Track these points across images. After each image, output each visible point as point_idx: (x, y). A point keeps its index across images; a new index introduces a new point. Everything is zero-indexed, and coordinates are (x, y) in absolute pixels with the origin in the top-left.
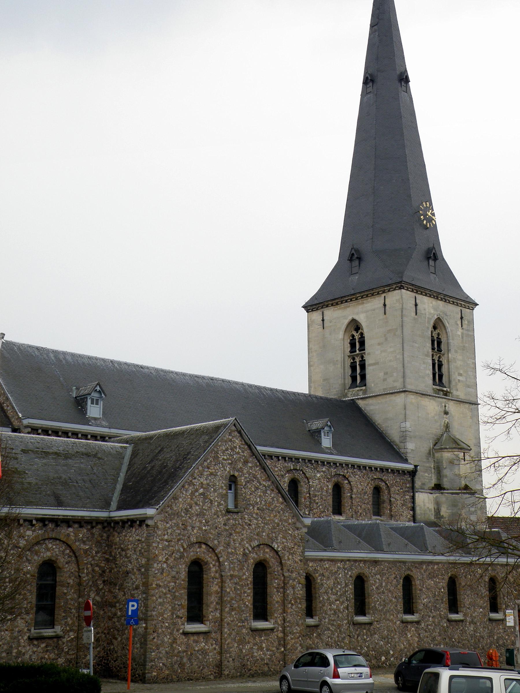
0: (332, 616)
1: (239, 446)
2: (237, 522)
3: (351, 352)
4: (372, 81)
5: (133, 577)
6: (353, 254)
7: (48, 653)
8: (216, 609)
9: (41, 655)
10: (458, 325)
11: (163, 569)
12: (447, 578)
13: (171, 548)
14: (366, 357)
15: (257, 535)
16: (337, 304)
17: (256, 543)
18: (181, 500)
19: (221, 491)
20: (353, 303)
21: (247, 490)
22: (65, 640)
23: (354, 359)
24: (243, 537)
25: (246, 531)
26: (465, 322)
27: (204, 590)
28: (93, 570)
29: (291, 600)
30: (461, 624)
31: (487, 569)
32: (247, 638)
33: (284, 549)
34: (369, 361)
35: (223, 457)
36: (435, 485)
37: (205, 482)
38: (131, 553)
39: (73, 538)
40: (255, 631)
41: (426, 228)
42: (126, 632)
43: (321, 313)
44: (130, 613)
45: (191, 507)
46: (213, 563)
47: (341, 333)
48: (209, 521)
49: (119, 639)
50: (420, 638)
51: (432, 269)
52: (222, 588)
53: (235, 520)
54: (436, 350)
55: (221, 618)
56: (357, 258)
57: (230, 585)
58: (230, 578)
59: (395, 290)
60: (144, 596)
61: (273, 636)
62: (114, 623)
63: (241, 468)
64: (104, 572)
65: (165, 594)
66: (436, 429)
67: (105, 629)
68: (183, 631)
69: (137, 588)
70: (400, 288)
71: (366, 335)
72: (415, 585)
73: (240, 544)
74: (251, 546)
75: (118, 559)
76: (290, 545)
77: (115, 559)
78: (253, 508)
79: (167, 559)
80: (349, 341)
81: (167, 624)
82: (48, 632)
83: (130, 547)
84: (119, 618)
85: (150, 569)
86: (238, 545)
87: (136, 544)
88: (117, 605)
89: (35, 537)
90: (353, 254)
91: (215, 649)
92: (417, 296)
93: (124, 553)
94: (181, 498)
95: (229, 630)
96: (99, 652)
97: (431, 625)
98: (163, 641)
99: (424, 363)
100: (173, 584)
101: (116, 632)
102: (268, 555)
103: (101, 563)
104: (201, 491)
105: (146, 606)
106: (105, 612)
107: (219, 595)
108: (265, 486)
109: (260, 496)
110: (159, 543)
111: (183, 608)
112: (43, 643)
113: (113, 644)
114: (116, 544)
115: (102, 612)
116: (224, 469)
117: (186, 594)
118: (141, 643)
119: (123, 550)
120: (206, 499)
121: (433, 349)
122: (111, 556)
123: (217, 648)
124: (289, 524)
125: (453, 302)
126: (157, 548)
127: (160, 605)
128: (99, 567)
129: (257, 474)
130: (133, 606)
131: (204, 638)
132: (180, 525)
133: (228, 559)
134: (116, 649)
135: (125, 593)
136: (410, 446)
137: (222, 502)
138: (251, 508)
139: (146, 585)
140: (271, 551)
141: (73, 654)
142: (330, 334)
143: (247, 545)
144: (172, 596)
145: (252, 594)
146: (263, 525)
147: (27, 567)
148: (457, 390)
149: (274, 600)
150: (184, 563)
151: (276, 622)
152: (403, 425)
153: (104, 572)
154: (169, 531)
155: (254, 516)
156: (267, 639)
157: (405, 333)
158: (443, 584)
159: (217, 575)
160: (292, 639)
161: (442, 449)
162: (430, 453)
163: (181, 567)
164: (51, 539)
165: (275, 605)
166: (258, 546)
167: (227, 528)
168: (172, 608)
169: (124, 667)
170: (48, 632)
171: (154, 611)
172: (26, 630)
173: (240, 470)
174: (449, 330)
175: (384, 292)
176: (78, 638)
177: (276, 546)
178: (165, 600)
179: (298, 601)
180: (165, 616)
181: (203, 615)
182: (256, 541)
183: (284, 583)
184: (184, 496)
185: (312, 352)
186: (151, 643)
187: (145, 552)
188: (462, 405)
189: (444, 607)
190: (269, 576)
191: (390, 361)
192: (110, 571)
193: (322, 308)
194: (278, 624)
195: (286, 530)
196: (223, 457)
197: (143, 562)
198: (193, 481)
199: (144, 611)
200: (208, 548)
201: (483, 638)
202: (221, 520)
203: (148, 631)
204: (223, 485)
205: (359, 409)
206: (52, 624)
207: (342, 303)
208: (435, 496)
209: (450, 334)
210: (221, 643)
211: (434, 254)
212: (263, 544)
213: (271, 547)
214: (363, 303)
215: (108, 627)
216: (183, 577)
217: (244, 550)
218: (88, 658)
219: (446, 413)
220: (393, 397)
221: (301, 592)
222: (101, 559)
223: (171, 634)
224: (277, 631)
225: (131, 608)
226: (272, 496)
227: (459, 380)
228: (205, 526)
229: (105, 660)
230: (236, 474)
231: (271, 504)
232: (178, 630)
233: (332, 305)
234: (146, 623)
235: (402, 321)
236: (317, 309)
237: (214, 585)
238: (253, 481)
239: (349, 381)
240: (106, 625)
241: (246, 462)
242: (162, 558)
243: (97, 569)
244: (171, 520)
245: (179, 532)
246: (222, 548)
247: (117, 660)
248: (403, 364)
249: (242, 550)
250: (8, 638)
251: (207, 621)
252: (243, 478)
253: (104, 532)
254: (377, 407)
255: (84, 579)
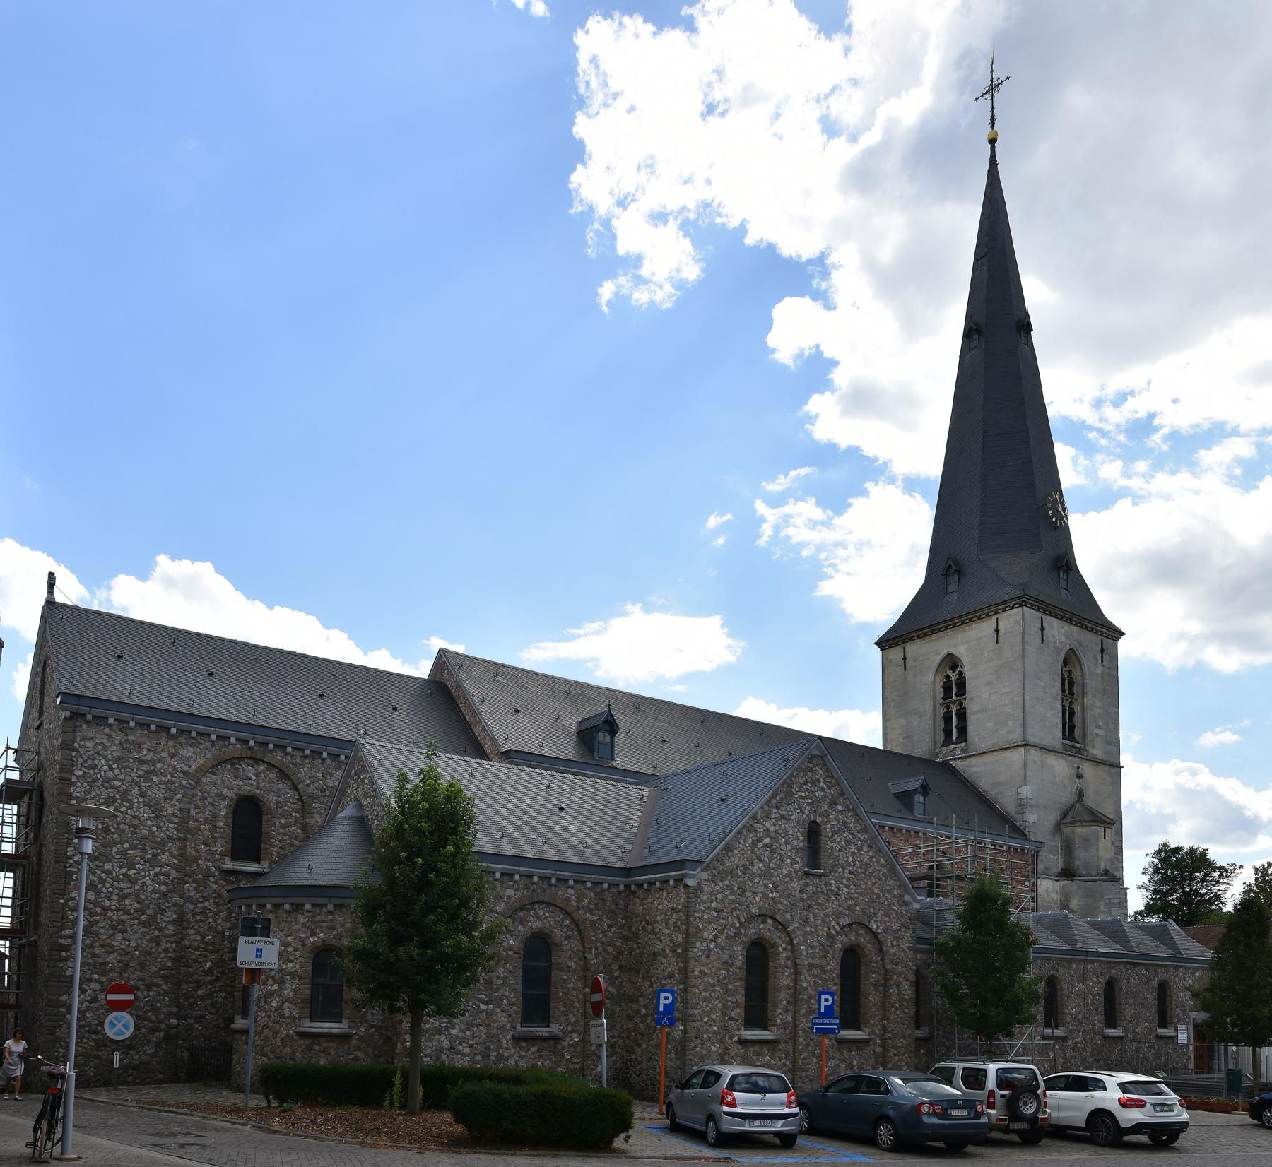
0: (948, 1027)
1: (824, 779)
2: (819, 889)
3: (944, 699)
4: (979, 331)
5: (664, 961)
6: (950, 567)
7: (542, 1060)
8: (788, 1011)
9: (532, 1062)
10: (1097, 659)
11: (710, 950)
12: (1103, 980)
13: (721, 921)
14: (965, 704)
15: (849, 909)
16: (926, 635)
17: (846, 921)
18: (736, 852)
19: (796, 842)
20: (950, 632)
21: (834, 845)
22: (565, 1043)
23: (948, 707)
24: (827, 911)
25: (833, 903)
26: (1106, 657)
27: (769, 983)
28: (605, 951)
29: (895, 1003)
30: (1119, 1041)
31: (1156, 972)
32: (830, 1051)
33: (886, 931)
34: (971, 708)
35: (799, 793)
36: (1062, 869)
37: (773, 828)
38: (660, 927)
39: (575, 904)
40: (843, 1042)
41: (1055, 527)
42: (654, 1036)
43: (902, 650)
44: (661, 1009)
45: (752, 864)
46: (784, 946)
47: (931, 673)
48: (778, 886)
49: (644, 1046)
50: (1066, 1058)
51: (1063, 584)
52: (796, 981)
53: (817, 886)
54: (1067, 693)
55: (794, 1023)
56: (956, 570)
57: (809, 978)
58: (808, 967)
59: (1013, 608)
60: (681, 987)
61: (868, 1051)
62: (637, 1024)
63: (826, 811)
64: (620, 953)
65: (713, 986)
66: (1066, 796)
67: (623, 1032)
68: (739, 1039)
69: (670, 976)
70: (1021, 606)
71: (967, 675)
72: (1062, 990)
73: (823, 921)
74: (838, 924)
75: (642, 936)
76: (895, 926)
77: (637, 936)
78: (843, 870)
79: (716, 937)
80: (941, 684)
81: (715, 1028)
82: (543, 1031)
83: (659, 918)
84: (644, 1017)
85: (691, 949)
86: (820, 922)
87: (669, 913)
88: (641, 999)
89: (520, 899)
90: (950, 567)
91: (785, 1065)
92: (1044, 617)
93: (650, 927)
94: (736, 849)
95: (805, 1040)
96: (615, 1062)
97: (1081, 1043)
98: (709, 1051)
99: (1052, 709)
100: (724, 972)
101: (639, 1037)
102: (863, 938)
103: (616, 941)
104: (767, 840)
105: (685, 1002)
106: (623, 1009)
107: (792, 991)
108: (860, 839)
109: (853, 854)
110: (703, 912)
111: (738, 1006)
112: (534, 1045)
113: (635, 1053)
114: (638, 915)
115: (618, 1009)
116: (801, 811)
117: (744, 986)
118: (677, 1054)
119: (648, 923)
120: (774, 853)
121: (1063, 691)
122: (630, 931)
123: (787, 1063)
124: (894, 896)
125: (1092, 629)
126: (700, 919)
127: (705, 1001)
128: (614, 946)
129: (849, 821)
130: (666, 998)
131: (769, 1050)
132: (736, 889)
133: (805, 941)
134: (639, 1059)
135: (652, 984)
136: (1031, 817)
137: (798, 859)
138: (840, 870)
139: (685, 972)
140: (866, 933)
141: (577, 1063)
142: (915, 677)
143: (833, 923)
144: (722, 989)
145: (839, 993)
146: (856, 895)
147: (508, 940)
148: (1094, 747)
149: (870, 1001)
150: (740, 944)
151: (872, 1032)
152: (1021, 790)
153: (620, 953)
154: (719, 896)
155: (845, 881)
156: (859, 1055)
157: (1026, 665)
158: (1098, 990)
159: (789, 963)
160: (895, 1055)
161: (1074, 822)
162: (1057, 828)
163: (736, 949)
164: (542, 903)
165: (871, 1009)
166: (849, 925)
167: (805, 896)
168: (723, 1005)
169: (652, 1084)
170: (543, 1031)
171: (696, 1009)
172: (508, 1026)
173: (825, 814)
174: (1086, 665)
175: (996, 613)
176: (585, 1042)
177: (875, 927)
178: (713, 994)
179: (905, 1004)
180: (713, 1016)
181: (767, 1017)
182: (846, 918)
183: (886, 980)
184: (741, 846)
185: (887, 702)
186: (693, 1052)
187: (682, 924)
188: (1100, 768)
189: (1097, 1019)
190: (863, 968)
191: (1004, 706)
192: (630, 954)
193: (904, 642)
194: (875, 1034)
195: (889, 905)
196: (799, 793)
197: (680, 939)
198: (755, 825)
199: (681, 1008)
200: (777, 923)
201: (1147, 1060)
202: (796, 885)
203: (687, 1035)
204: (799, 835)
205: (953, 771)
206: (546, 1020)
207: (933, 633)
208: (1062, 883)
209: (1087, 672)
210: (794, 1057)
211: (1067, 562)
212: (856, 923)
213: (867, 927)
214: (964, 631)
215: (627, 1029)
216: (739, 963)
217: (829, 929)
218: (599, 1069)
219: (1079, 776)
220: (1007, 754)
221: (909, 992)
222: (617, 936)
223: (721, 1041)
224: (874, 1045)
225: (662, 1002)
226: (870, 854)
227: (1097, 734)
228: (772, 893)
229: (624, 1073)
230: (819, 820)
231: (867, 866)
232: (731, 1038)
233: (918, 637)
234: (685, 1026)
235: (1023, 650)
236: (897, 645)
237: (785, 977)
238: (844, 832)
239: (940, 737)
240: (625, 1027)
241: (833, 803)
242: (709, 935)
243: (610, 949)
244: (721, 881)
245: (733, 898)
246: (797, 925)
247: (640, 1074)
248: (1024, 707)
249: (826, 929)
250: (483, 1036)
251: (773, 1026)
252: (829, 826)
253: (620, 899)
254: (983, 768)
255: (592, 962)
